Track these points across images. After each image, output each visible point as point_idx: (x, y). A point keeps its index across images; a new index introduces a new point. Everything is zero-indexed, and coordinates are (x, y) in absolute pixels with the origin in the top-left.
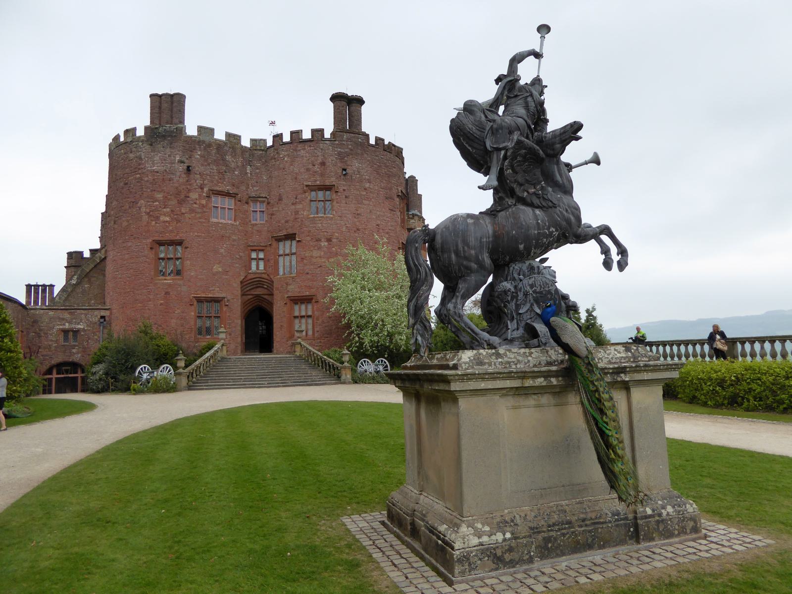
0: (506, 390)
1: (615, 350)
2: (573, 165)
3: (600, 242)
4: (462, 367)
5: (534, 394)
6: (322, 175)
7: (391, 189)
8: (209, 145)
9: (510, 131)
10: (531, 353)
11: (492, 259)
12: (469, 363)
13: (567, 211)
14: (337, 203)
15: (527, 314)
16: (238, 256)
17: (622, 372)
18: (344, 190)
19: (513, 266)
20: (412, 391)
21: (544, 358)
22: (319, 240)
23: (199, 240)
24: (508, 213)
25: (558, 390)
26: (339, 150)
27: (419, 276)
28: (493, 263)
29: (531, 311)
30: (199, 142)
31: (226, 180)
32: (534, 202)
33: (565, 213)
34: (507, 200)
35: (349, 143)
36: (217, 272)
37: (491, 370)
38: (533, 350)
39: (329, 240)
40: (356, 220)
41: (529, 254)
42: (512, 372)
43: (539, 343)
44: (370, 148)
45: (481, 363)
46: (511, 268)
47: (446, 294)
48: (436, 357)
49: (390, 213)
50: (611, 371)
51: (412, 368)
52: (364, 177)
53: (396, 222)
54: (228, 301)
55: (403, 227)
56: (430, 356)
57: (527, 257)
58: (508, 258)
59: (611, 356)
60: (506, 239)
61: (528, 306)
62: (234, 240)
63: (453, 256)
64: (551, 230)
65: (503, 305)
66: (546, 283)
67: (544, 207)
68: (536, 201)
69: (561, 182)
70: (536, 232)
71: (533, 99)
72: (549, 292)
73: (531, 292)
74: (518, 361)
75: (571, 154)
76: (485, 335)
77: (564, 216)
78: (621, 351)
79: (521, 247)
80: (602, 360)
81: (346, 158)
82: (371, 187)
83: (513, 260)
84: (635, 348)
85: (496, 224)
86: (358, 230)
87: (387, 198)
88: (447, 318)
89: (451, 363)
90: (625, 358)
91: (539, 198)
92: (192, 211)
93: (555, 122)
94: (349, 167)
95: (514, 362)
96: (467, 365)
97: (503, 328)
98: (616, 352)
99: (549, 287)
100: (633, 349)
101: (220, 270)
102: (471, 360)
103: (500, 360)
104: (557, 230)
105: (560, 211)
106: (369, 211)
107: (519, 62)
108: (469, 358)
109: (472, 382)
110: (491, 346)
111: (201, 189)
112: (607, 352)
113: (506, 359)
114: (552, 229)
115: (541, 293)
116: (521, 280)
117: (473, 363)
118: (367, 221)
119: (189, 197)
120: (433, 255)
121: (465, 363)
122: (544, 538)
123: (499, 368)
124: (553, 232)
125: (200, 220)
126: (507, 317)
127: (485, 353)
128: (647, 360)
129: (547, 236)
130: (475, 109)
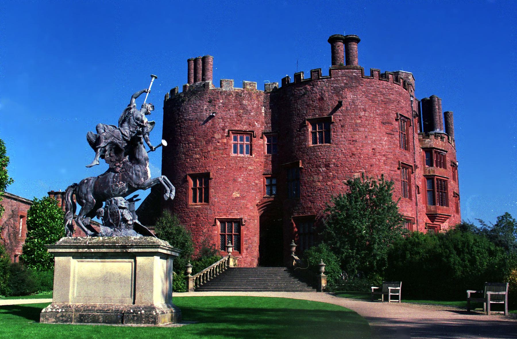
6: (321, 109)
7: (388, 115)
8: (230, 94)
14: (334, 132)
16: (253, 184)
18: (340, 120)
22: (319, 166)
23: (221, 171)
26: (335, 85)
30: (221, 92)
31: (244, 121)
35: (344, 78)
36: (236, 198)
39: (327, 166)
40: (351, 146)
44: (365, 80)
52: (359, 106)
53: (394, 144)
54: (245, 221)
62: (251, 170)
81: (341, 92)
82: (366, 115)
86: (353, 154)
87: (383, 123)
92: (216, 149)
94: (345, 100)
101: (238, 195)
106: (364, 137)
111: (223, 130)
118: (362, 146)
119: (214, 138)
122: (80, 315)
125: (223, 156)
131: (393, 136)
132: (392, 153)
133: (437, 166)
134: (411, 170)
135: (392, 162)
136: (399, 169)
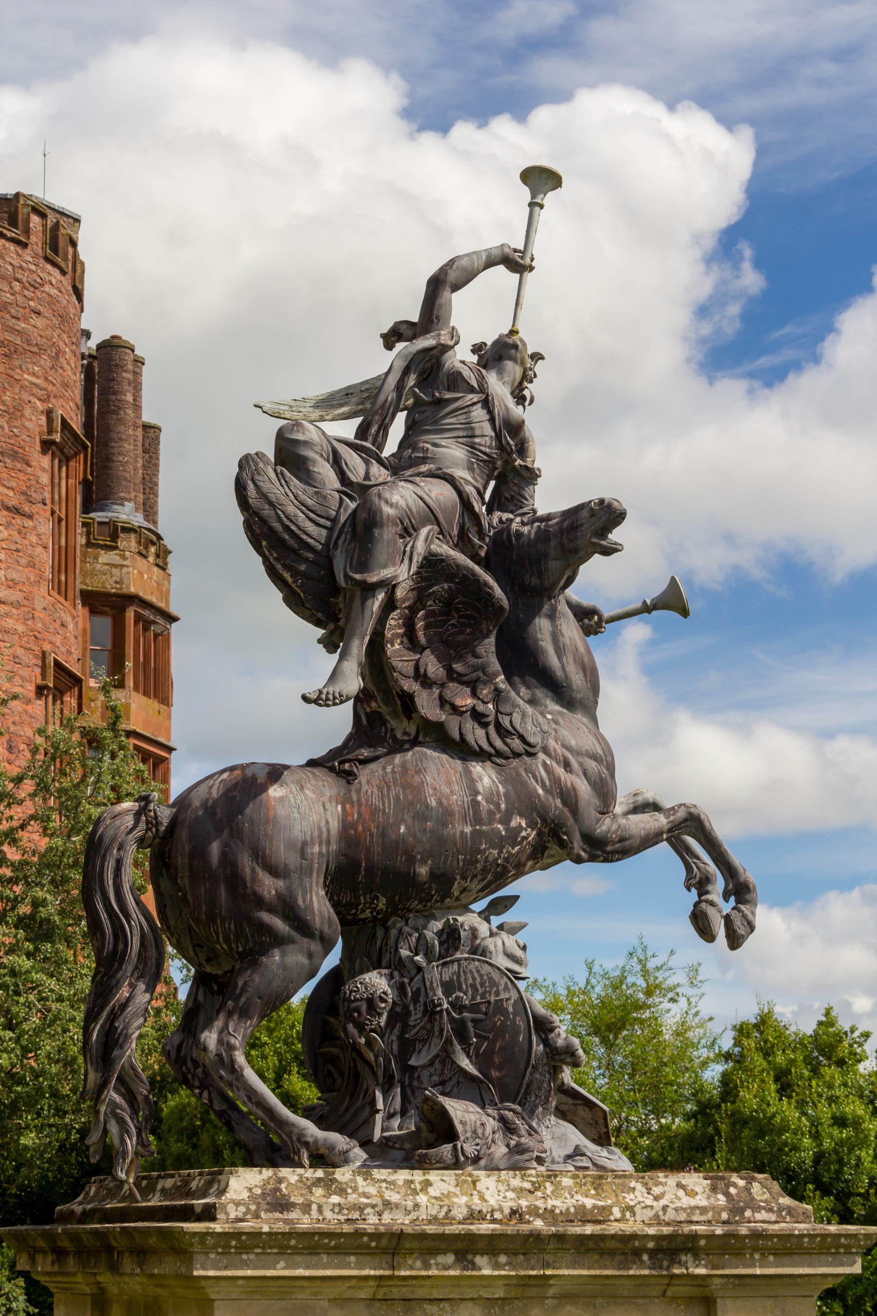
0: (348, 1284)
1: (679, 1185)
2: (606, 614)
3: (683, 851)
4: (227, 1214)
5: (431, 1301)
9: (405, 529)
10: (428, 1184)
11: (335, 905)
12: (246, 1205)
13: (567, 765)
15: (432, 1070)
17: (688, 1250)
19: (399, 925)
20: (88, 1290)
21: (464, 1200)
24: (389, 769)
25: (500, 1293)
27: (121, 946)
28: (338, 913)
29: (443, 1063)
32: (470, 738)
33: (560, 771)
34: (393, 723)
37: (305, 1223)
38: (434, 1176)
41: (446, 893)
42: (364, 1233)
43: (457, 1158)
45: (281, 1204)
46: (394, 932)
47: (201, 997)
48: (159, 1187)
49: (8, 525)
50: (651, 1245)
51: (86, 1217)
53: (32, 565)
55: (62, 589)
56: (144, 1183)
57: (442, 901)
58: (382, 903)
59: (663, 1202)
60: (377, 849)
61: (435, 1047)
63: (223, 892)
64: (513, 824)
65: (363, 1040)
66: (491, 979)
67: (499, 754)
68: (476, 735)
69: (559, 673)
70: (468, 830)
71: (490, 412)
72: (499, 1007)
73: (446, 1006)
74: (387, 1204)
75: (596, 581)
76: (311, 1129)
77: (556, 781)
78: (698, 1189)
79: (423, 871)
80: (634, 1214)
83: (397, 909)
84: (741, 1183)
85: (352, 803)
88: (199, 1071)
89: (199, 1203)
90: (703, 1210)
91: (485, 725)
93: (549, 498)
95: (373, 1206)
96: (242, 1209)
97: (363, 1107)
98: (681, 1193)
99: (497, 994)
100: (735, 1185)
102: (253, 1197)
103: (335, 1199)
104: (531, 825)
105: (545, 764)
107: (456, 288)
108: (250, 1190)
109: (252, 1257)
110: (323, 1158)
112: (657, 1190)
113: (352, 1198)
114: (517, 821)
115: (474, 1008)
116: (419, 969)
117: (258, 1204)
120: (165, 883)
121: (237, 1204)
123: (332, 1220)
124: (520, 828)
126: (374, 1074)
127: (293, 1179)
128: (773, 1217)
129: (500, 843)
130: (310, 454)
131: (29, 523)
132: (18, 605)
133: (136, 688)
134: (74, 703)
135: (20, 652)
136: (40, 691)
